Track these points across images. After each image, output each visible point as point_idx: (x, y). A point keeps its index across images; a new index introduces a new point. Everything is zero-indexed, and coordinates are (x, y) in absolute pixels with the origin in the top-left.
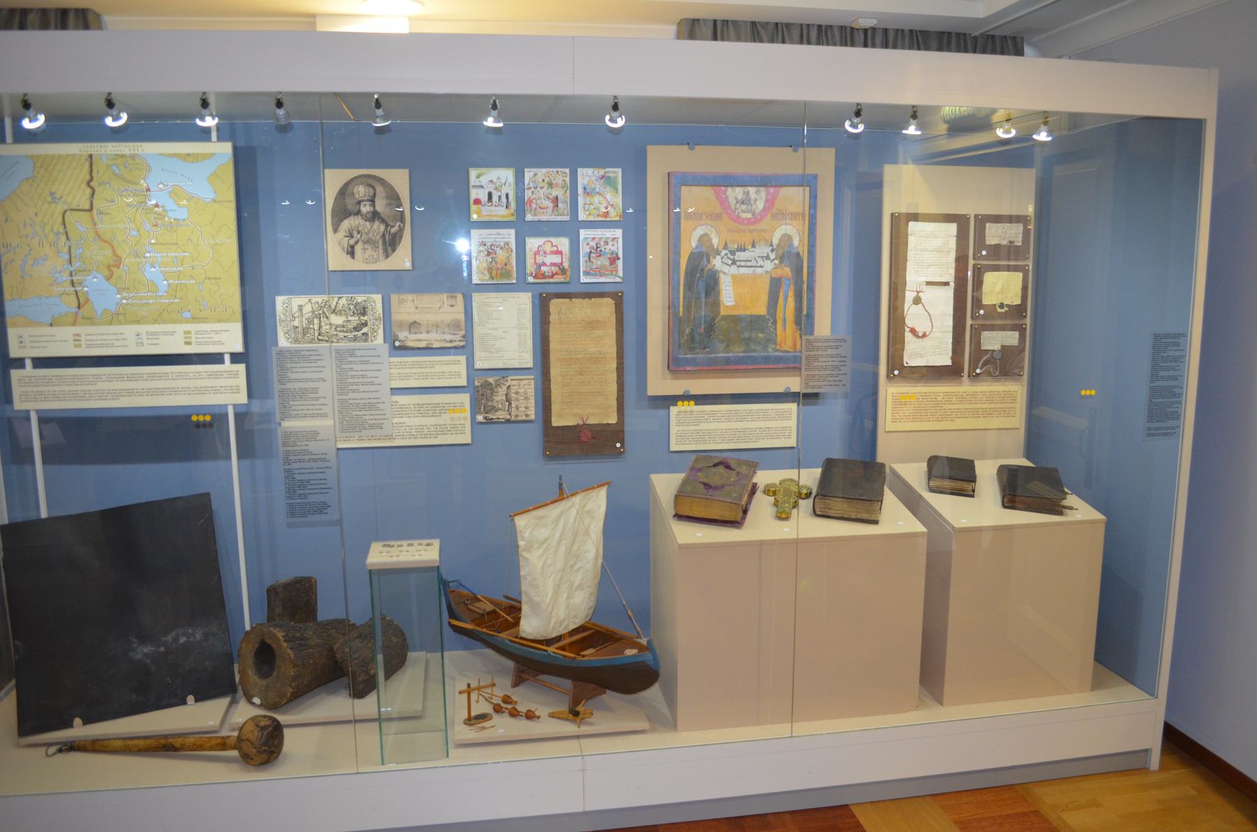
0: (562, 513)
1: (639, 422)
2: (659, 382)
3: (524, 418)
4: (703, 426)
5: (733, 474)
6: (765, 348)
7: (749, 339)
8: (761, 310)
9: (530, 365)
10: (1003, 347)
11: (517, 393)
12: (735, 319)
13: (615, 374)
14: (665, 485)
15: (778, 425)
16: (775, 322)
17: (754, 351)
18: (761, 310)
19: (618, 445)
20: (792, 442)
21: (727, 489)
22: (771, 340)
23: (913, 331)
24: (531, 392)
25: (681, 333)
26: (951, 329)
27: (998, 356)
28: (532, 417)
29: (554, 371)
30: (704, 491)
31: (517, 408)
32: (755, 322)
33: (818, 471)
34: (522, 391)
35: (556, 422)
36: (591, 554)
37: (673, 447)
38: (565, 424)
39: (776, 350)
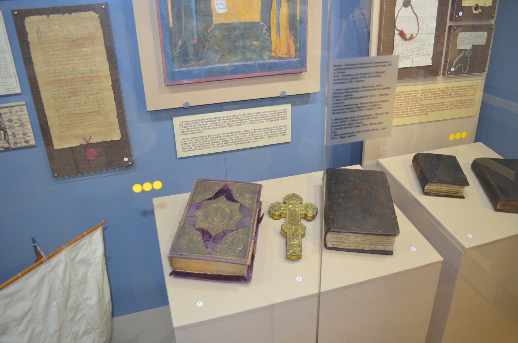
0: (43, 278)
1: (144, 138)
2: (158, 96)
3: (24, 144)
4: (207, 133)
5: (236, 206)
6: (261, 55)
7: (244, 47)
8: (256, 17)
9: (18, 90)
10: (473, 46)
11: (10, 121)
12: (228, 28)
13: (112, 92)
14: (169, 214)
15: (274, 126)
16: (269, 29)
17: (250, 59)
18: (256, 17)
19: (126, 159)
20: (288, 138)
21: (230, 236)
22: (266, 47)
23: (402, 34)
24: (25, 117)
25: (173, 45)
26: (434, 31)
27: (469, 55)
28: (33, 142)
29: (45, 95)
30: (201, 244)
31: (14, 135)
32: (249, 30)
33: (318, 177)
34: (15, 118)
35: (58, 145)
36: (94, 301)
37: (180, 154)
38: (68, 146)
39: (271, 57)
